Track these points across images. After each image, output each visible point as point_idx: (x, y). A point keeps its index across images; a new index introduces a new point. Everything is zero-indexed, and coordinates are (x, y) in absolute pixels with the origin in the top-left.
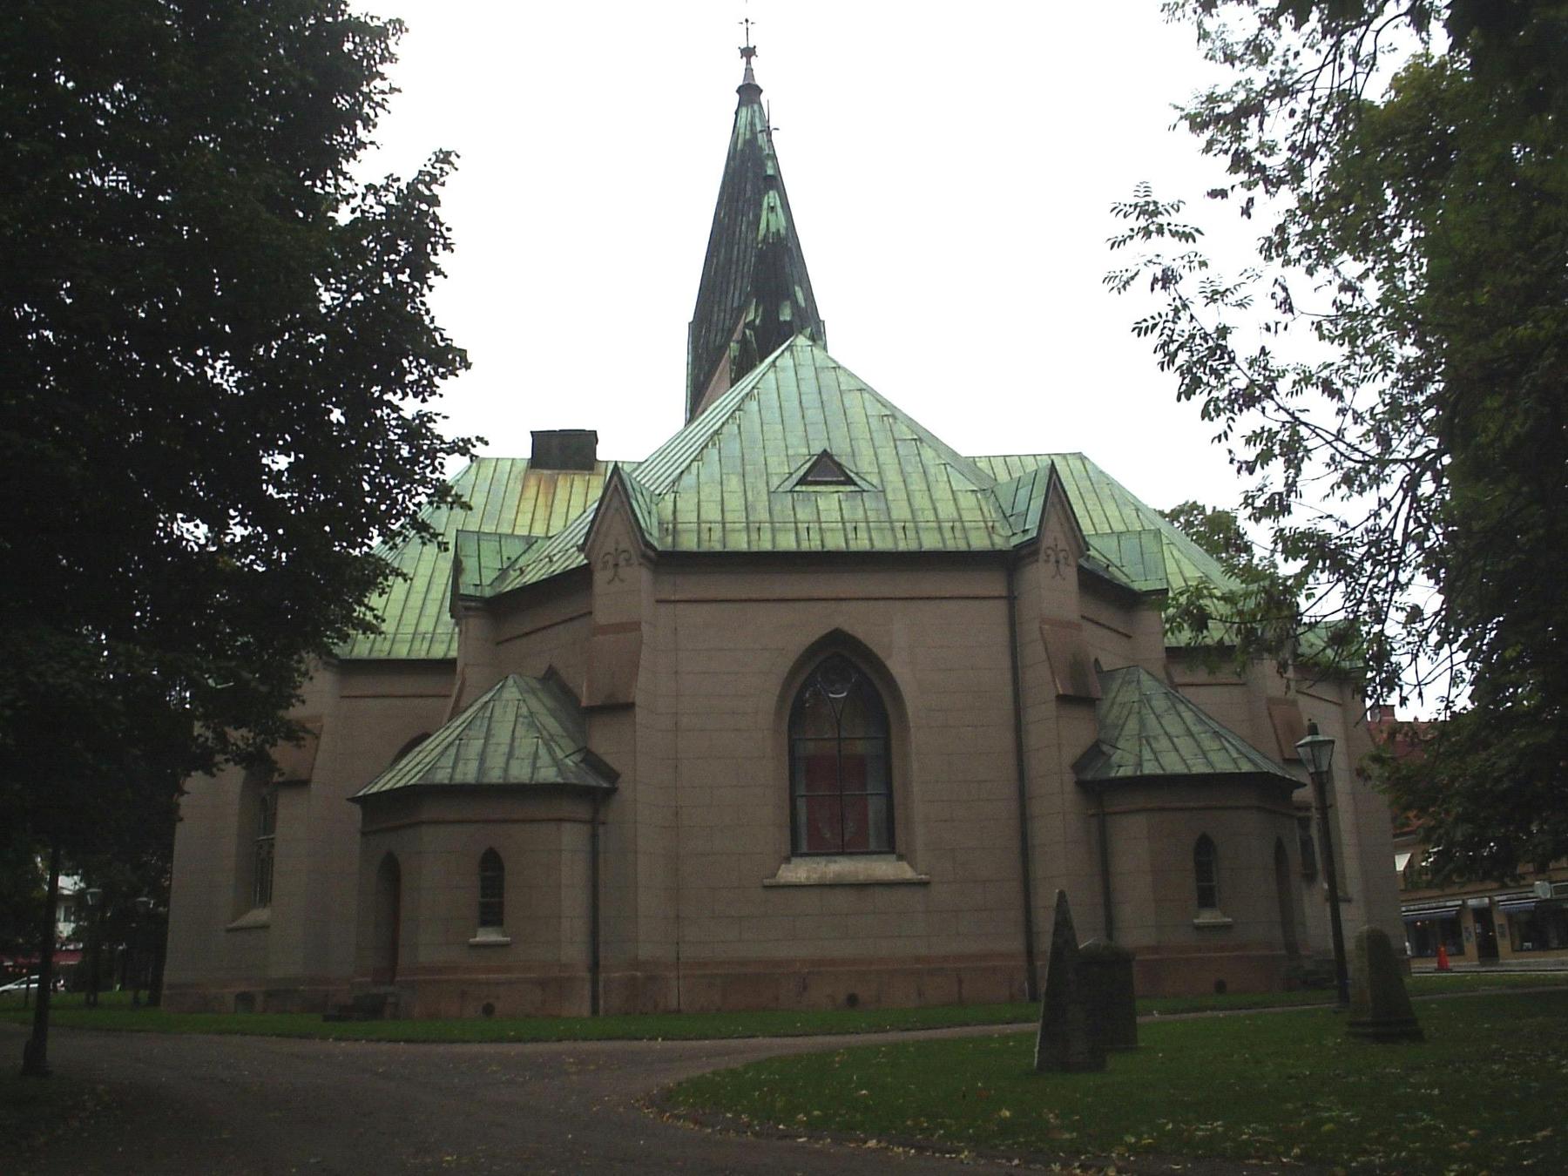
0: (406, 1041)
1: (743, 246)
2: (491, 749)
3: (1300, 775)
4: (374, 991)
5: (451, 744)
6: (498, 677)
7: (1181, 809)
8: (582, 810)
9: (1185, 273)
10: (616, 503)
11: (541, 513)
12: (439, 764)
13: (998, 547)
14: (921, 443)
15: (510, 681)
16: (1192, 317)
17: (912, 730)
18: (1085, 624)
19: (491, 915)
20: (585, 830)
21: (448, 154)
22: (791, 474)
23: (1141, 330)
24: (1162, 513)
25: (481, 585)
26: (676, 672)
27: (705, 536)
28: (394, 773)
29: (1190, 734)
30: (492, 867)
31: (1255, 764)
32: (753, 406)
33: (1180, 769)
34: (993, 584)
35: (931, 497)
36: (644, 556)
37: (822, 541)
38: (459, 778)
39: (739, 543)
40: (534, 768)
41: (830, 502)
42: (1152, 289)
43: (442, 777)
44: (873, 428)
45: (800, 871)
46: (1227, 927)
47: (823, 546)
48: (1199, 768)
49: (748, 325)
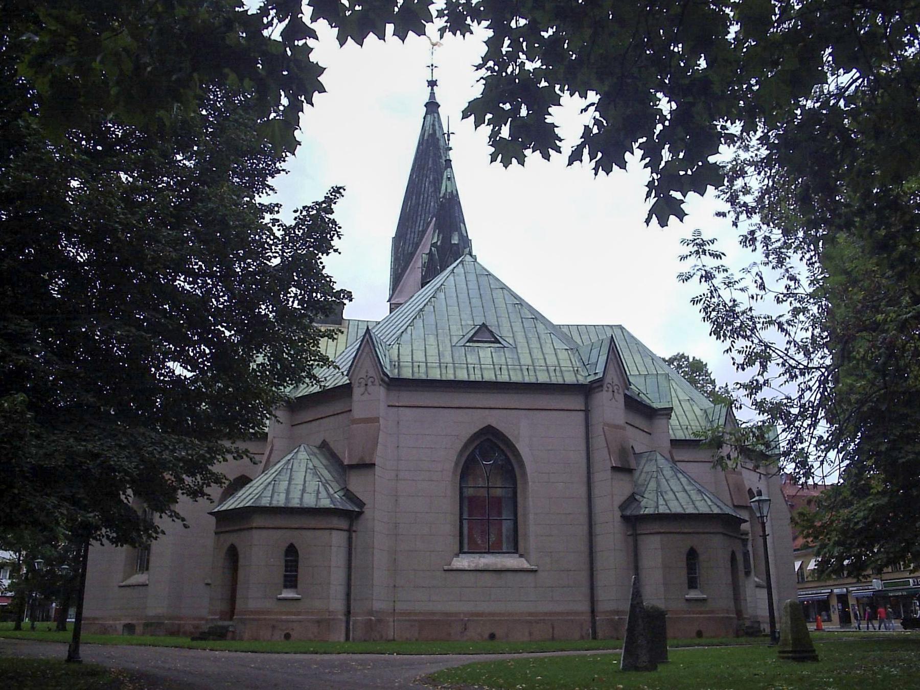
0: (252, 652)
1: (426, 196)
2: (292, 487)
3: (744, 515)
4: (220, 623)
5: (269, 483)
6: (293, 445)
7: (679, 533)
8: (344, 524)
9: (716, 273)
10: (367, 349)
12: (263, 495)
13: (580, 382)
15: (302, 448)
16: (719, 296)
17: (530, 483)
18: (628, 427)
19: (291, 581)
20: (344, 535)
21: (340, 188)
22: (464, 336)
23: (694, 301)
24: (664, 359)
27: (416, 369)
28: (235, 499)
29: (685, 491)
31: (721, 509)
32: (441, 295)
33: (679, 510)
34: (576, 402)
36: (382, 380)
37: (482, 375)
38: (275, 504)
39: (435, 375)
40: (318, 498)
41: (486, 353)
42: (701, 282)
43: (265, 502)
44: (510, 311)
45: (464, 562)
46: (704, 600)
47: (483, 378)
48: (690, 510)
49: (433, 245)
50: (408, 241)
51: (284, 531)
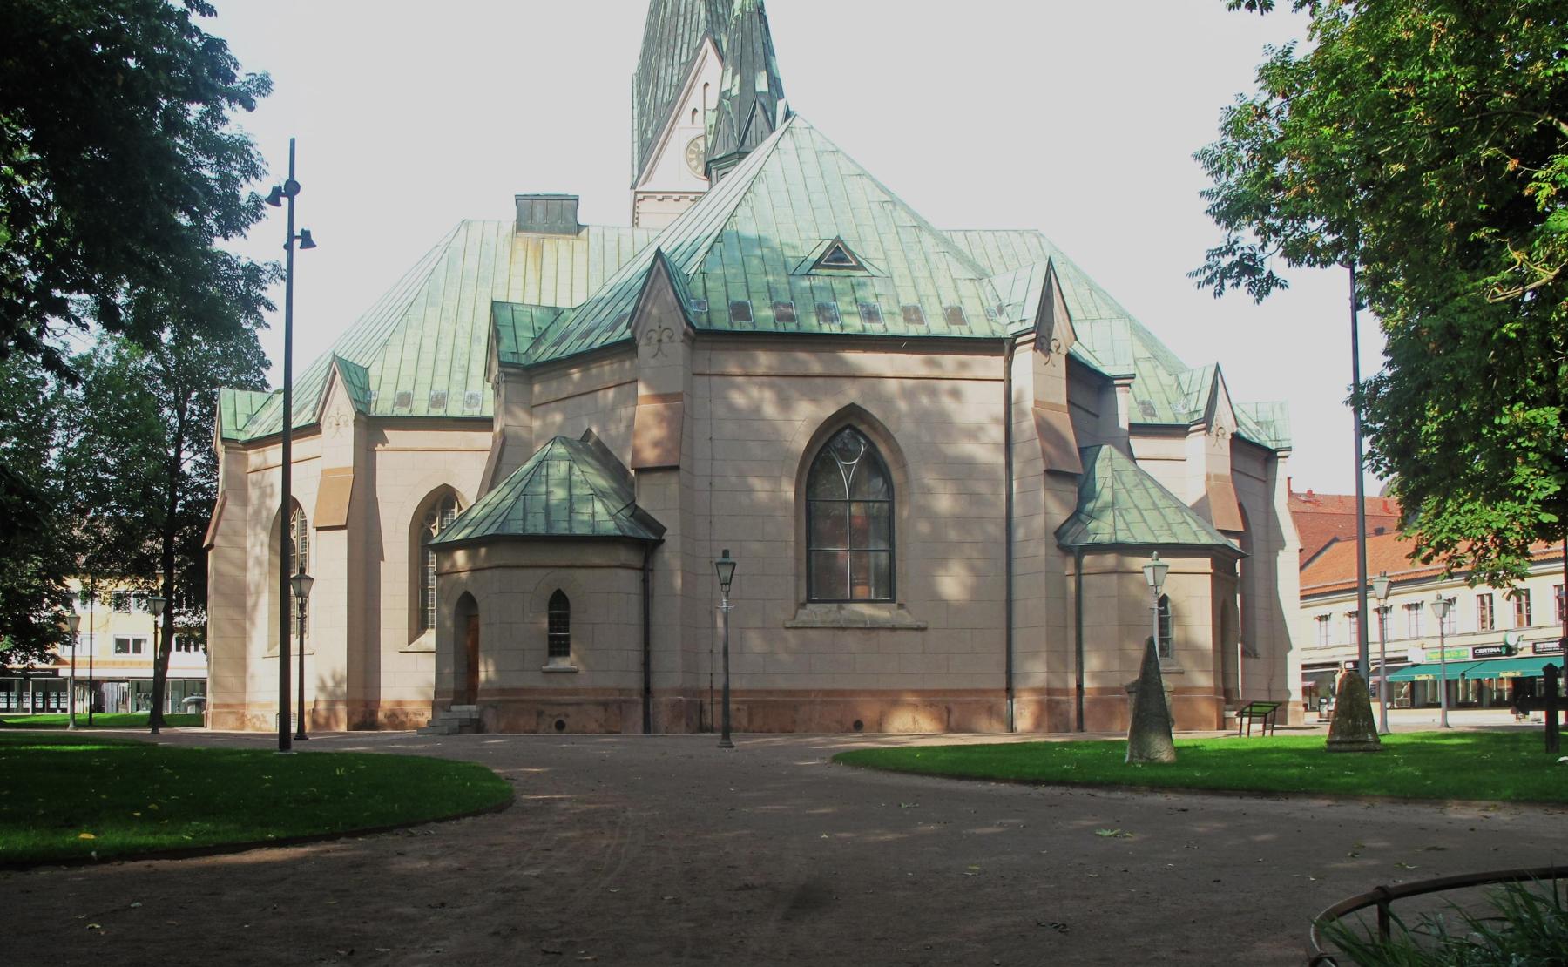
11: (532, 277)
13: (997, 335)
14: (920, 230)
25: (517, 352)
26: (711, 439)
30: (559, 604)
32: (760, 188)
35: (934, 284)
50: (661, 82)
51: (548, 571)
